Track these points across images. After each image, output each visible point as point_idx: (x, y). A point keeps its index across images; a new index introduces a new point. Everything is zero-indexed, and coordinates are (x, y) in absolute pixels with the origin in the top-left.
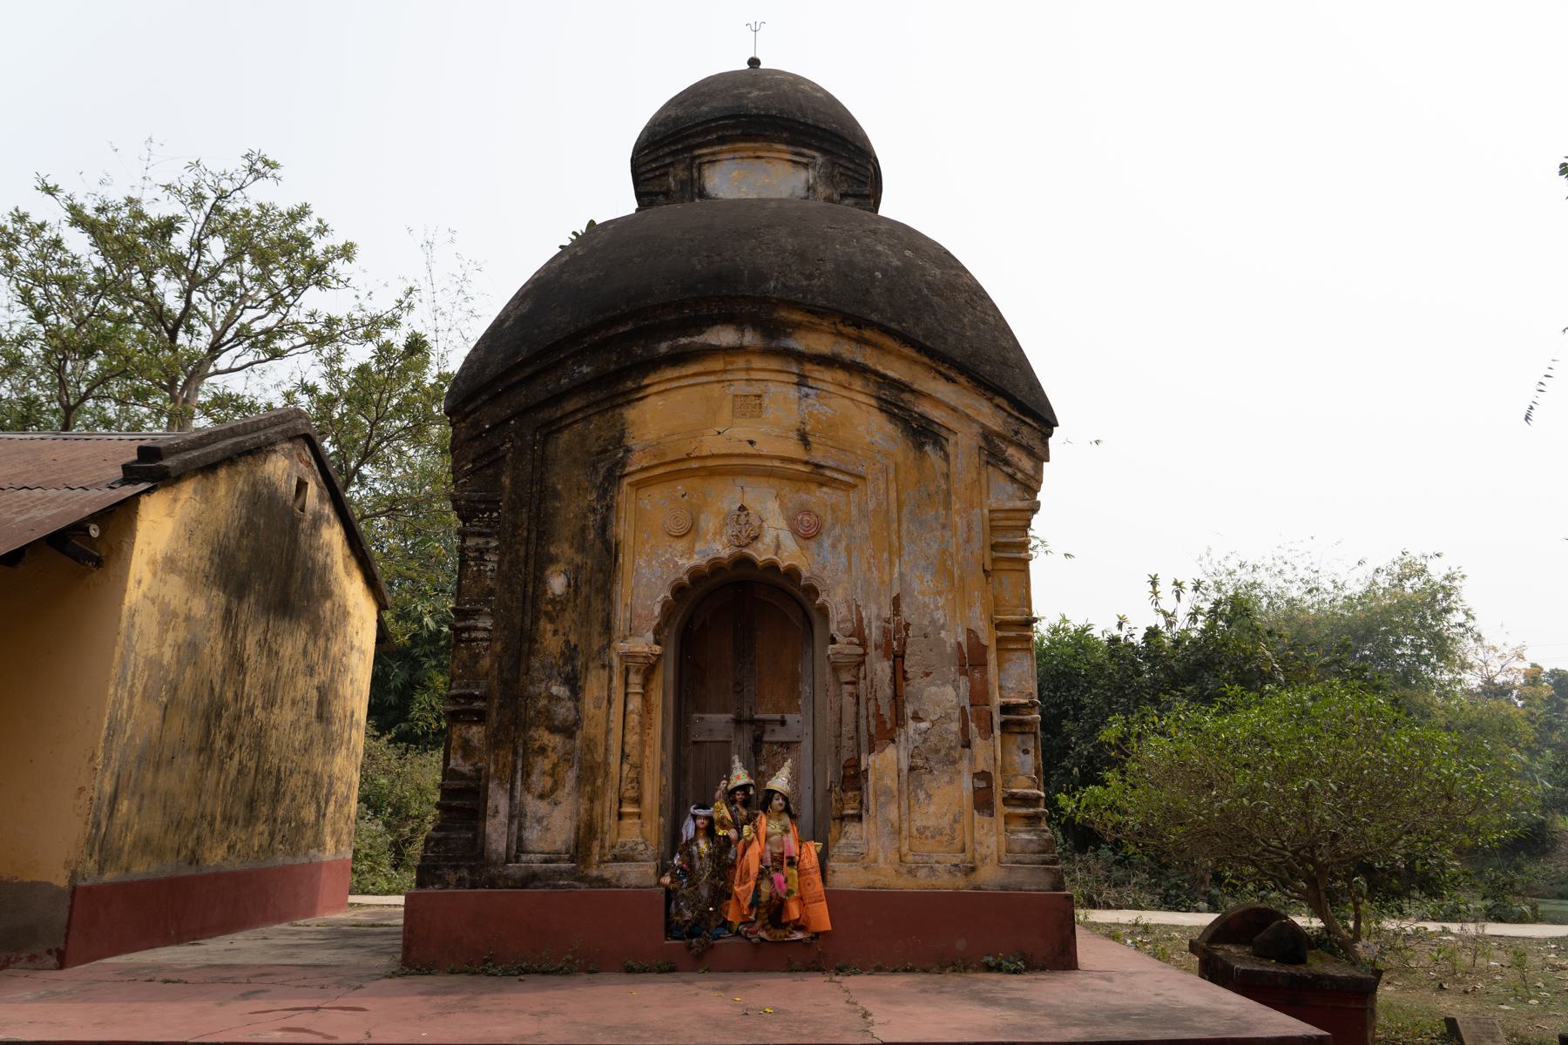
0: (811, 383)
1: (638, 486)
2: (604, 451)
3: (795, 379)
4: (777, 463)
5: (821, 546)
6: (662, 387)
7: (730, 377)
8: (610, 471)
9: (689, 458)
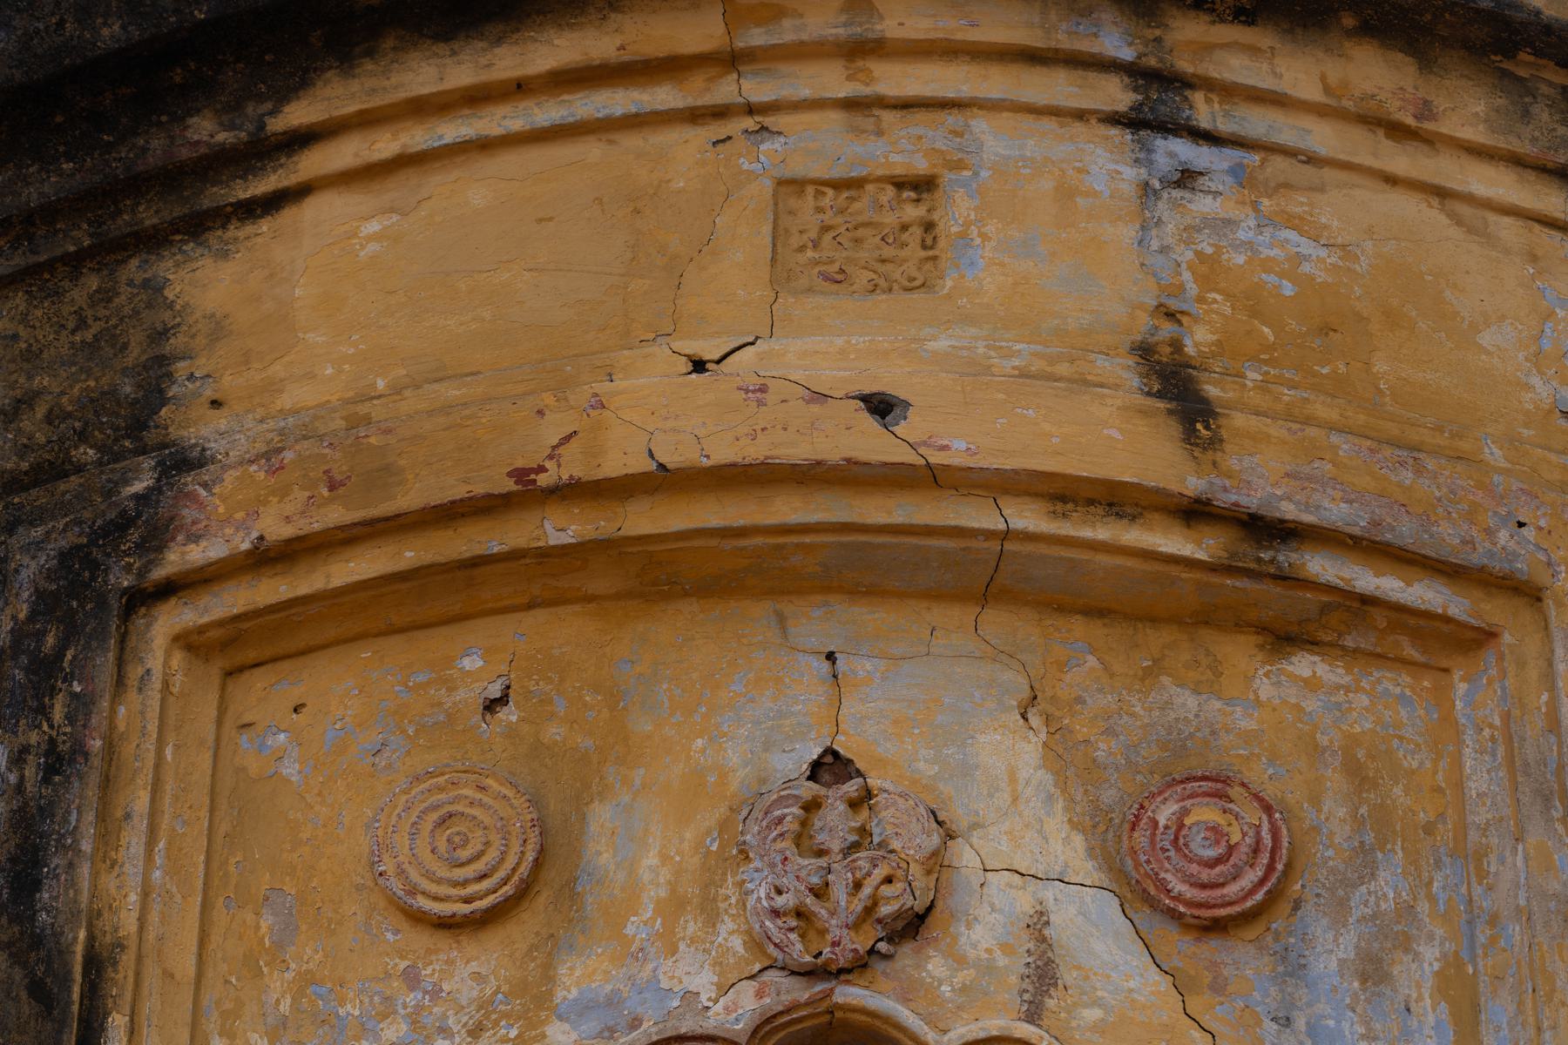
0: (1204, 111)
1: (234, 651)
2: (51, 471)
3: (1116, 95)
4: (1027, 517)
5: (1292, 968)
6: (384, 145)
7: (757, 89)
8: (75, 577)
9: (530, 491)
